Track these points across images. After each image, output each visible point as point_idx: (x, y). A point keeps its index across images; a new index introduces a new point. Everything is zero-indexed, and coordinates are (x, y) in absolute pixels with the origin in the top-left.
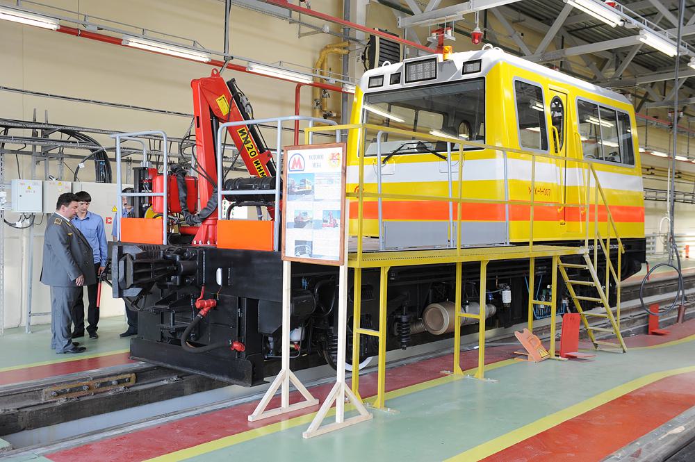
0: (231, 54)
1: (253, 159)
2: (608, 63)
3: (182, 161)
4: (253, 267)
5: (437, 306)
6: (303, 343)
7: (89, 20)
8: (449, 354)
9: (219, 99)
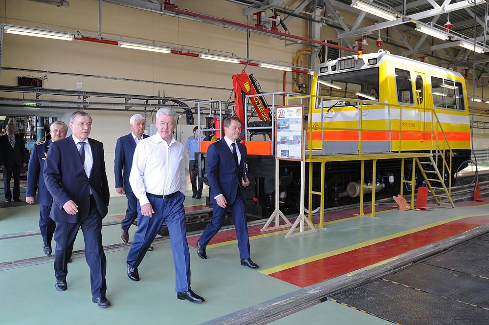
0: (250, 58)
1: (262, 112)
2: (460, 52)
3: (227, 113)
4: (260, 164)
5: (354, 183)
6: (286, 199)
7: (184, 47)
8: (358, 208)
9: (245, 85)
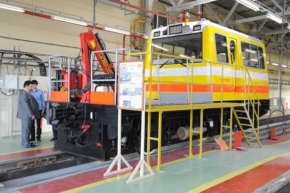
0: (96, 22)
1: (106, 67)
2: (254, 26)
3: (76, 67)
4: (106, 111)
6: (126, 143)
7: (37, 8)
9: (91, 41)
